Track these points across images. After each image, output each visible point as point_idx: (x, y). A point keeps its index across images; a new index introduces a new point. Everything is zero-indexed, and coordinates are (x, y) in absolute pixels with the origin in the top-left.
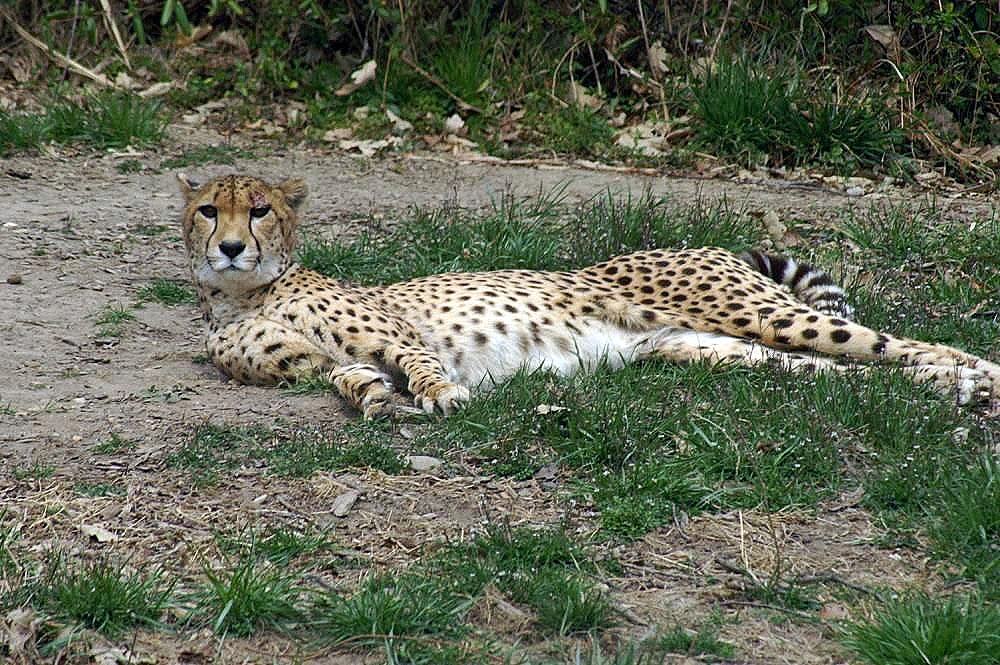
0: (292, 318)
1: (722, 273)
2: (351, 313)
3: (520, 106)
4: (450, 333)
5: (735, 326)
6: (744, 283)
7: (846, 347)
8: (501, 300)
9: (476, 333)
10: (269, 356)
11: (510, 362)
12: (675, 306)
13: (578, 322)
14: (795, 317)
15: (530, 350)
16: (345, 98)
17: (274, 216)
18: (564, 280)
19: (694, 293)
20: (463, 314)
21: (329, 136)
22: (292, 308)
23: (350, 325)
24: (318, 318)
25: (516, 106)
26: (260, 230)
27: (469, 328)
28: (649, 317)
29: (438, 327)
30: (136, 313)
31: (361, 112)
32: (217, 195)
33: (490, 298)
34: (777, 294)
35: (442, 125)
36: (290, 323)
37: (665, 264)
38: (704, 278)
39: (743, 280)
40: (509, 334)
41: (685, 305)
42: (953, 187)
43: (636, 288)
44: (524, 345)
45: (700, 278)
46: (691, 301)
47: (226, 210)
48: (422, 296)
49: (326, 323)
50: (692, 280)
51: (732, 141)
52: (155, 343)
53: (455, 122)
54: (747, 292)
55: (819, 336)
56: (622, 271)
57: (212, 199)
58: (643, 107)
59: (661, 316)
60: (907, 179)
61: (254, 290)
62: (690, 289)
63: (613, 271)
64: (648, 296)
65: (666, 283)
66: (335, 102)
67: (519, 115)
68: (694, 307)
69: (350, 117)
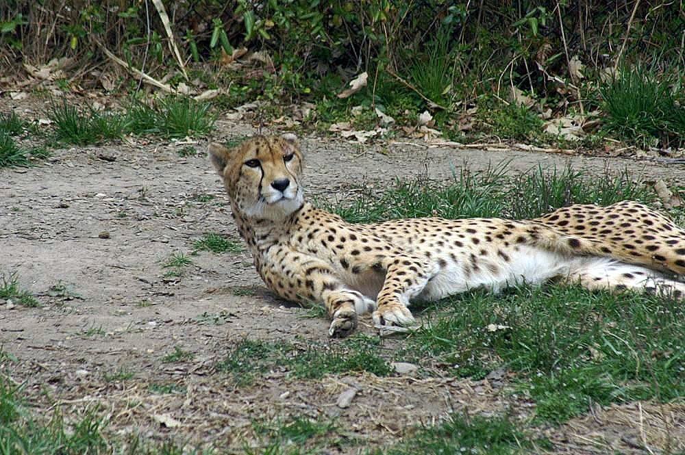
16: (345, 100)
20: (432, 245)
27: (435, 255)
30: (193, 259)
32: (257, 151)
35: (416, 119)
44: (467, 272)
47: (268, 159)
52: (207, 281)
53: (426, 117)
67: (473, 111)
69: (349, 113)
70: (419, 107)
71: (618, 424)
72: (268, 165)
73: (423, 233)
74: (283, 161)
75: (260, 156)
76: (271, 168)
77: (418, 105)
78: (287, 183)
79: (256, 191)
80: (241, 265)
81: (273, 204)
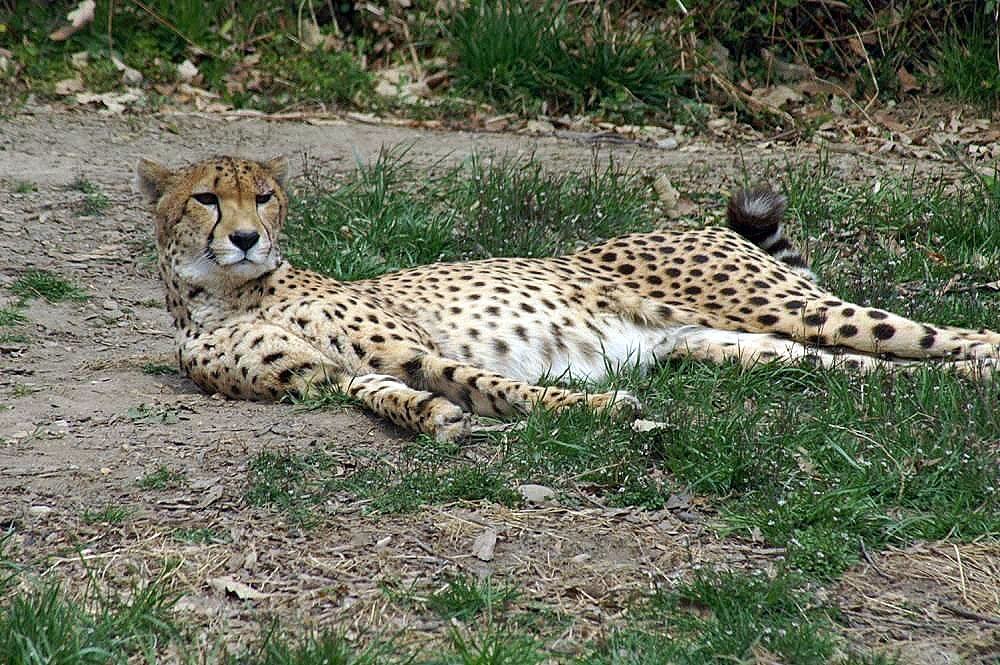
0: (302, 323)
1: (737, 261)
2: (373, 319)
3: (254, 49)
4: (467, 340)
5: (761, 325)
6: (763, 270)
7: (890, 344)
8: (515, 298)
9: (496, 340)
10: (268, 366)
11: (531, 373)
12: (689, 299)
13: (596, 322)
14: (827, 312)
15: (554, 358)
16: (61, 43)
17: (276, 202)
18: (562, 269)
19: (710, 285)
20: (477, 316)
21: (62, 87)
22: (302, 312)
23: (373, 333)
24: (335, 327)
25: (250, 50)
26: (266, 218)
27: (487, 334)
28: (665, 313)
29: (452, 332)
30: (22, 312)
31: (79, 59)
32: (217, 181)
33: (501, 296)
34: (800, 283)
35: (174, 72)
36: (300, 327)
37: (670, 250)
38: (720, 266)
39: (761, 268)
40: (531, 340)
41: (700, 299)
42: (751, 135)
43: (641, 277)
44: (547, 353)
45: (714, 267)
46: (706, 295)
47: (231, 196)
48: (425, 294)
49: (345, 332)
50: (704, 268)
51: (502, 86)
52: (69, 349)
53: (187, 69)
54: (768, 282)
55: (896, 335)
56: (622, 258)
57: (211, 184)
58: (385, 47)
59: (678, 313)
60: (699, 128)
61: (242, 287)
62: (704, 281)
63: (610, 257)
64: (656, 288)
65: (675, 273)
66: (49, 47)
67: (253, 59)
68: (711, 302)
69: (70, 65)
70: (170, 53)
71: (916, 579)
72: (230, 206)
73: (449, 295)
74: (254, 203)
75: (219, 189)
76: (235, 211)
77: (169, 49)
78: (253, 239)
79: (203, 241)
80: (99, 322)
81: (227, 266)
